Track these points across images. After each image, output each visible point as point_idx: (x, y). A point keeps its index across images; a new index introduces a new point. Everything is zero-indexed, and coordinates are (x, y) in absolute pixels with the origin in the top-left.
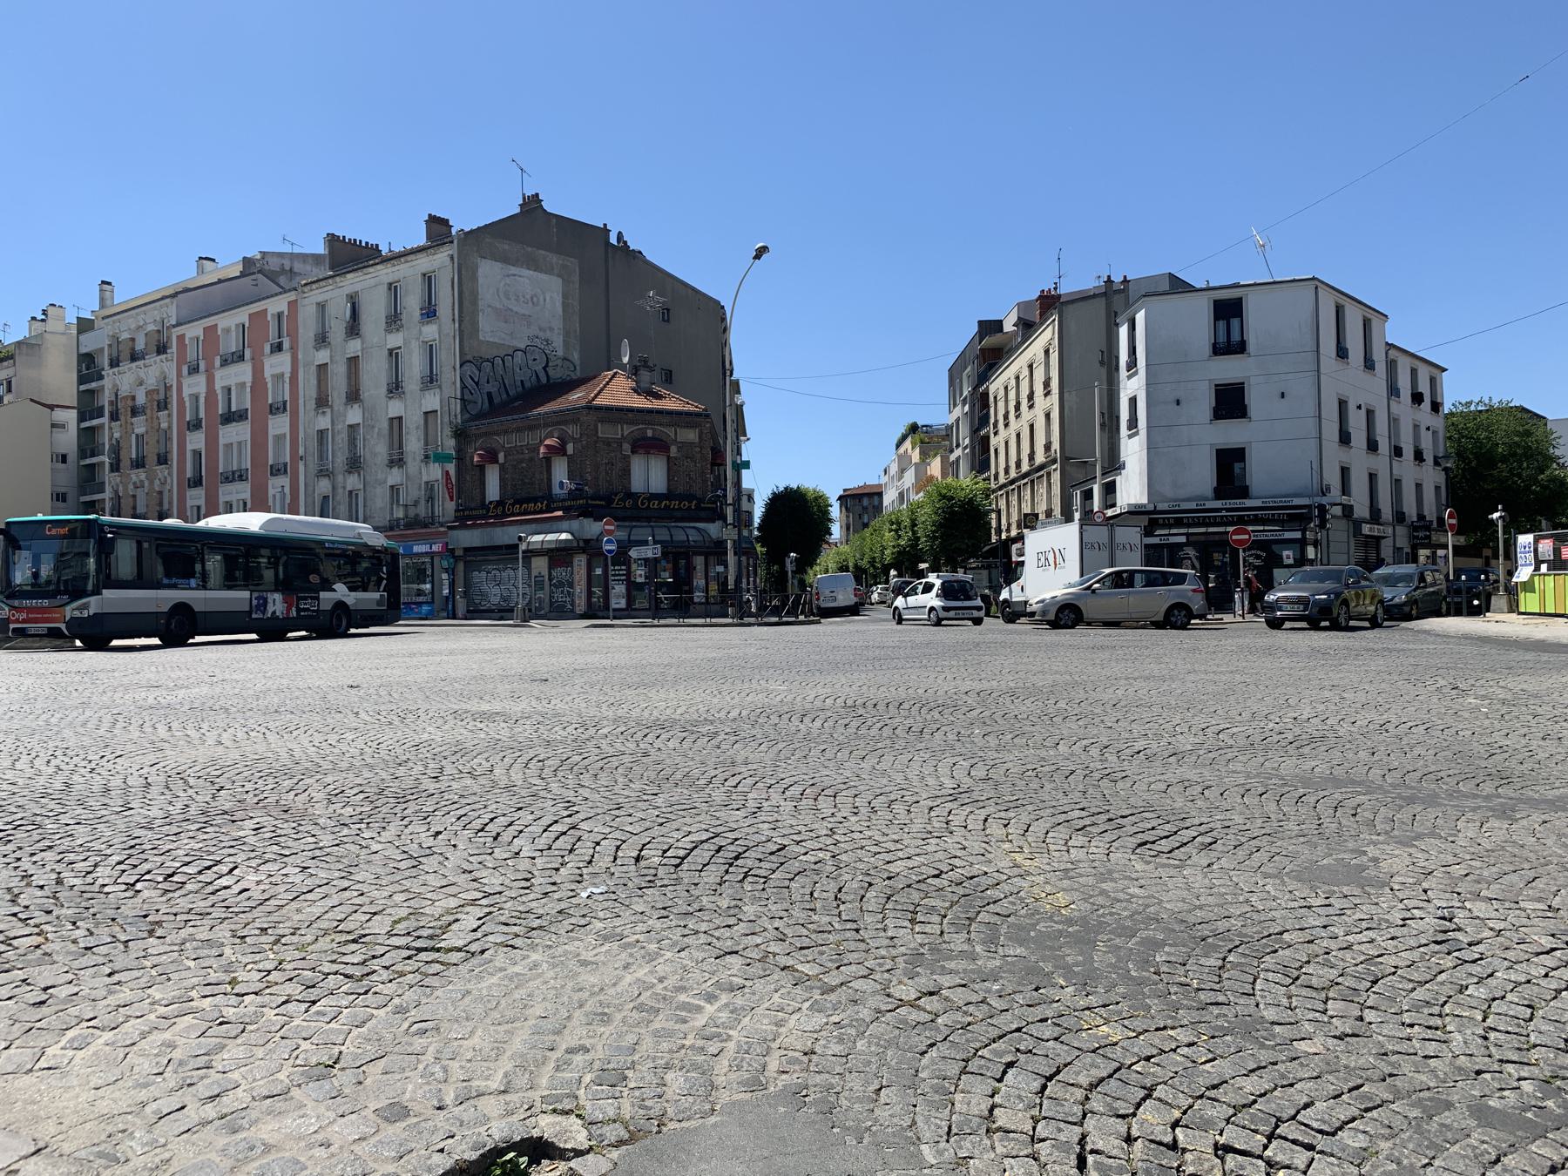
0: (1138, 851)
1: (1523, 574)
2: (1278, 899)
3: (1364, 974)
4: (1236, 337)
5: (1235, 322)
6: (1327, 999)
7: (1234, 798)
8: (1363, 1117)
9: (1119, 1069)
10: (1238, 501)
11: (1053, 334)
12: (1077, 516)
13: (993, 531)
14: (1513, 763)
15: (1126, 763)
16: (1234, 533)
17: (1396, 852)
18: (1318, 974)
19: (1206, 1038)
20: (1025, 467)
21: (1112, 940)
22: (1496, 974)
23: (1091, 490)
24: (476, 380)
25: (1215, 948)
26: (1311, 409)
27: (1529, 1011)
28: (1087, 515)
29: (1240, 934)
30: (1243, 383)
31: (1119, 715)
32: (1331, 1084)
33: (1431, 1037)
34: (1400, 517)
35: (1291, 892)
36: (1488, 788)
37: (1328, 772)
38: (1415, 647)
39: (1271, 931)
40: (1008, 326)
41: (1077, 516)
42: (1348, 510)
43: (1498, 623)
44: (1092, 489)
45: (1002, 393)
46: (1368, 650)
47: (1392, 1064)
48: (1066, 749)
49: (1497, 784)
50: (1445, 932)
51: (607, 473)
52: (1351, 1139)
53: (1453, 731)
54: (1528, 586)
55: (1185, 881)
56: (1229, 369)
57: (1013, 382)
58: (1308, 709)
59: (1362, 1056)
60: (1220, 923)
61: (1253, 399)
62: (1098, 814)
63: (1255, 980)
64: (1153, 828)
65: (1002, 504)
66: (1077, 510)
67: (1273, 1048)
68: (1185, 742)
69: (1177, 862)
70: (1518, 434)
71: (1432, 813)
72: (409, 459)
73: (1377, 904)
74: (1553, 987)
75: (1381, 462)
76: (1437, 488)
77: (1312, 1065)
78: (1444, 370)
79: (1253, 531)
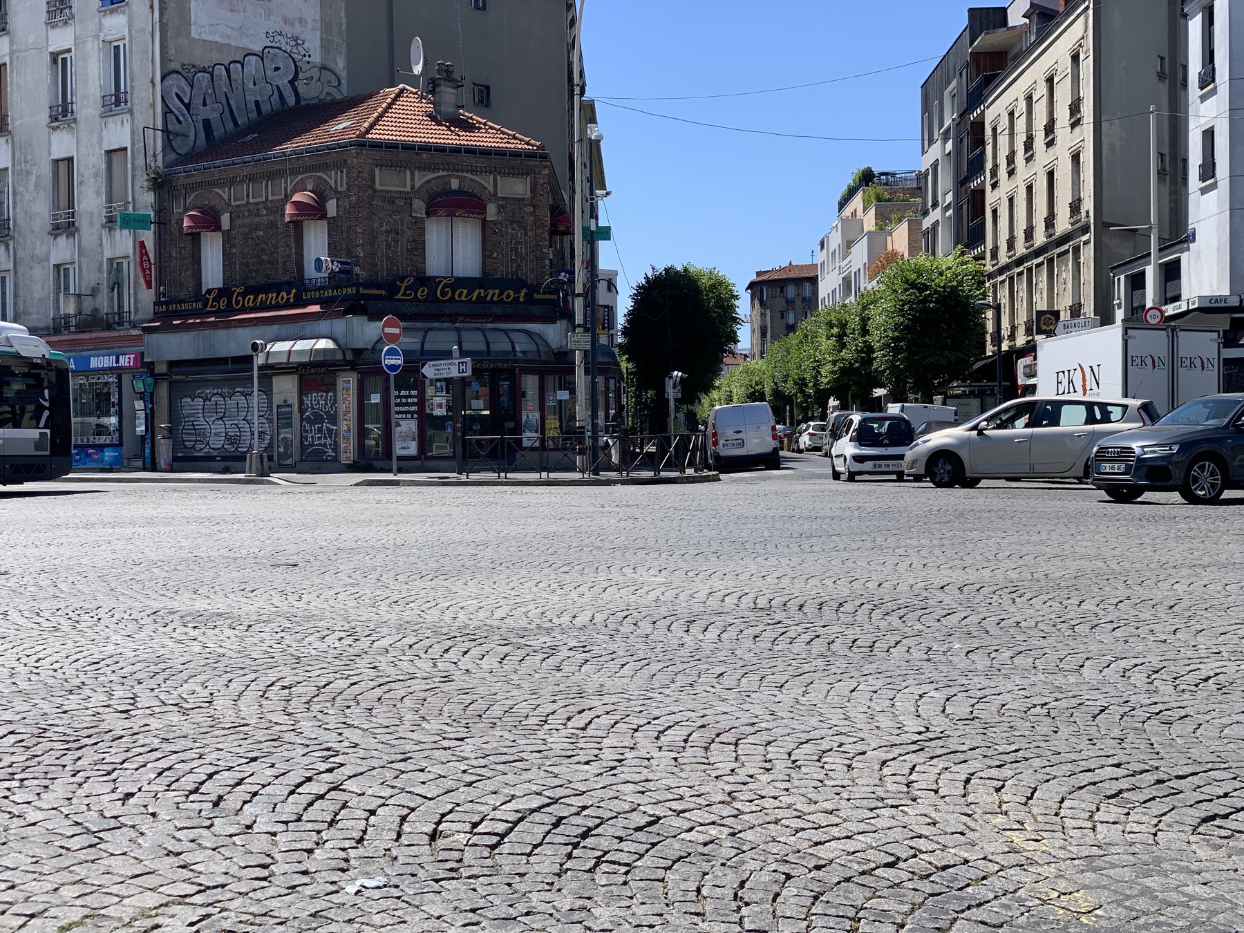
0: (1201, 829)
11: (1086, 31)
12: (1120, 314)
13: (988, 338)
15: (1186, 695)
20: (1040, 239)
23: (1142, 274)
24: (186, 101)
28: (1136, 314)
40: (1016, 18)
41: (1120, 314)
44: (1143, 273)
45: (1005, 121)
51: (388, 246)
57: (1022, 106)
62: (1142, 772)
64: (1226, 795)
65: (1003, 296)
66: (1119, 306)
72: (83, 222)
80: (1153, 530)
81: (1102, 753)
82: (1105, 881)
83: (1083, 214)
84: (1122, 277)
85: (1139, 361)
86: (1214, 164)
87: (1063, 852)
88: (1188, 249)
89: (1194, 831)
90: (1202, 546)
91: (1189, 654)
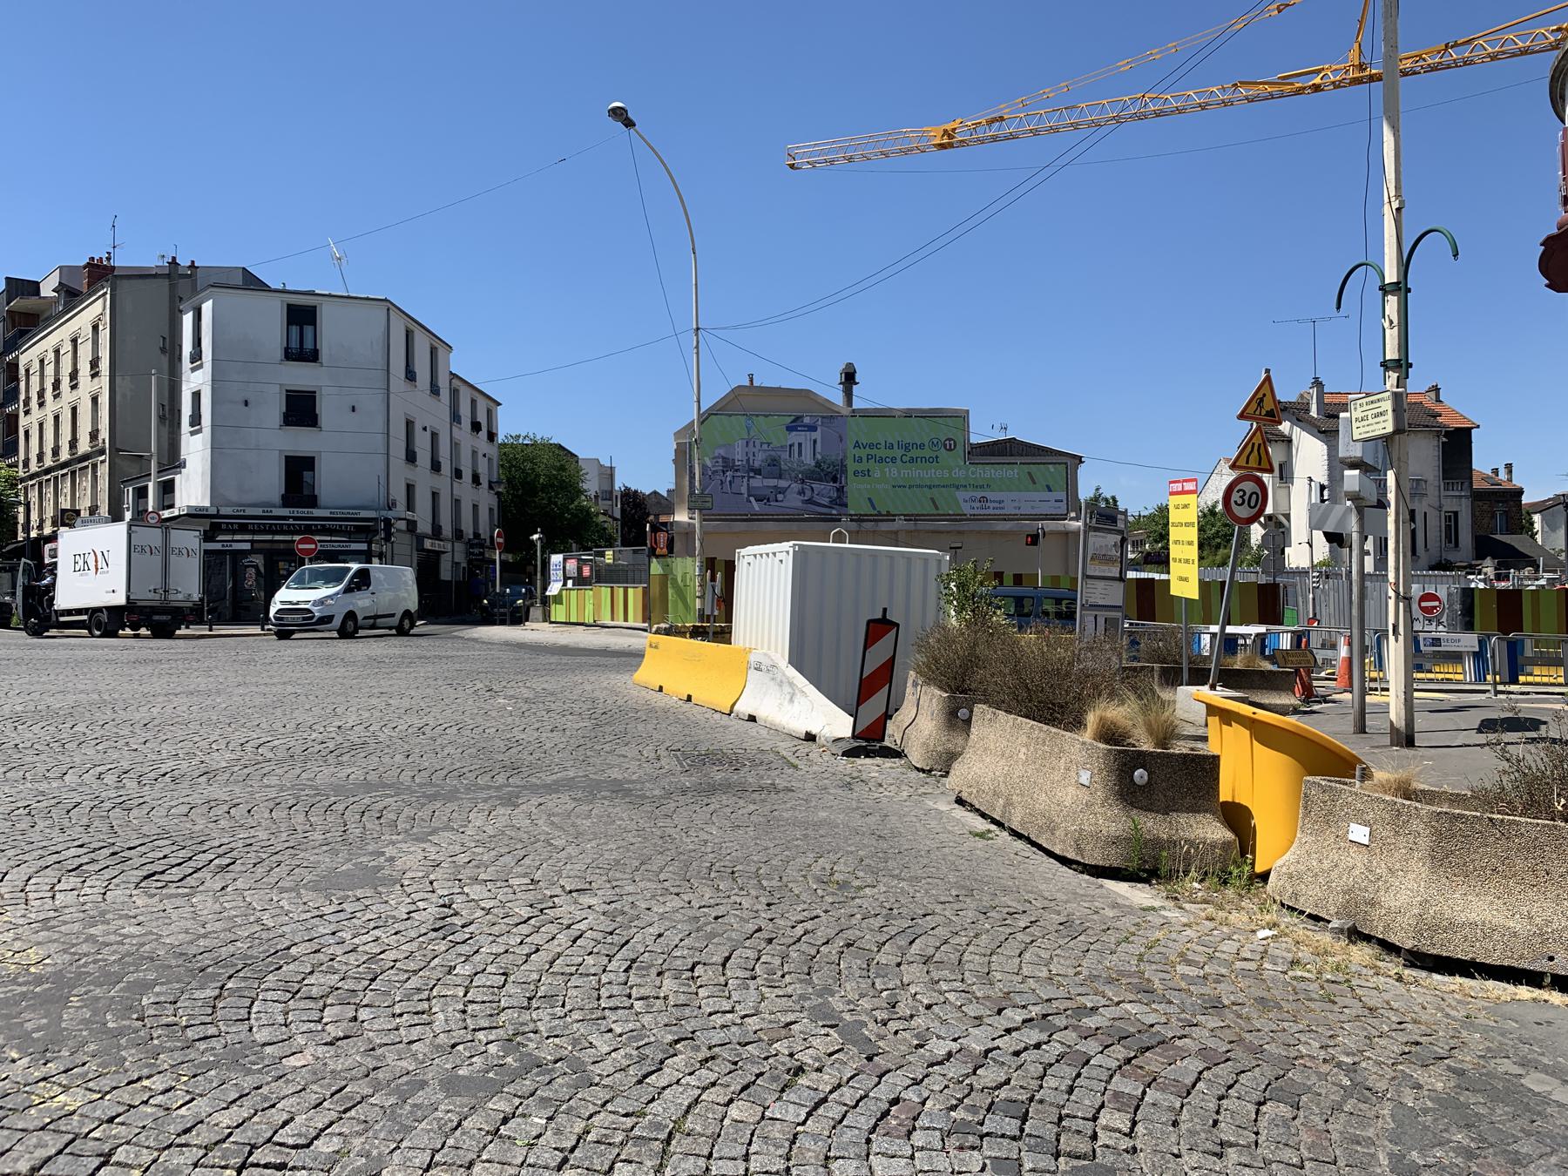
0: (142, 885)
1: (554, 589)
2: (292, 912)
3: (365, 973)
4: (308, 345)
5: (308, 330)
6: (325, 1006)
7: (261, 813)
8: (341, 1118)
9: (73, 1141)
10: (306, 510)
11: (104, 309)
12: (128, 515)
13: (20, 528)
14: (525, 754)
15: (147, 788)
16: (301, 542)
17: (411, 849)
18: (318, 983)
19: (186, 1078)
20: (65, 455)
21: (90, 991)
22: (482, 950)
23: (146, 488)
25: (214, 977)
26: (380, 425)
27: (503, 978)
28: (140, 515)
29: (246, 957)
30: (315, 392)
31: (149, 735)
32: (316, 1091)
33: (417, 1022)
34: (458, 534)
35: (305, 903)
36: (501, 779)
37: (362, 778)
38: (462, 653)
39: (279, 947)
40: (47, 290)
41: (128, 515)
42: (412, 525)
43: (534, 632)
44: (146, 487)
45: (36, 366)
46: (420, 658)
47: (378, 1058)
48: (76, 779)
49: (508, 774)
50: (443, 918)
52: (324, 1146)
53: (481, 729)
54: (558, 599)
55: (193, 909)
56: (301, 376)
57: (51, 356)
58: (354, 718)
59: (353, 1056)
60: (224, 949)
61: (325, 409)
62: (100, 849)
63: (253, 1003)
64: (165, 857)
65: (34, 496)
66: (128, 509)
67: (260, 1071)
68: (219, 760)
69: (186, 890)
70: (554, 467)
71: (451, 806)
73: (386, 902)
74: (525, 952)
75: (443, 482)
76: (491, 510)
77: (298, 1079)
78: (499, 404)
79: (319, 541)
80: (142, 670)
81: (69, 838)
82: (56, 936)
83: (101, 441)
84: (131, 489)
85: (140, 549)
86: (200, 416)
87: (23, 919)
88: (180, 473)
89: (137, 886)
90: (177, 680)
91: (154, 758)
